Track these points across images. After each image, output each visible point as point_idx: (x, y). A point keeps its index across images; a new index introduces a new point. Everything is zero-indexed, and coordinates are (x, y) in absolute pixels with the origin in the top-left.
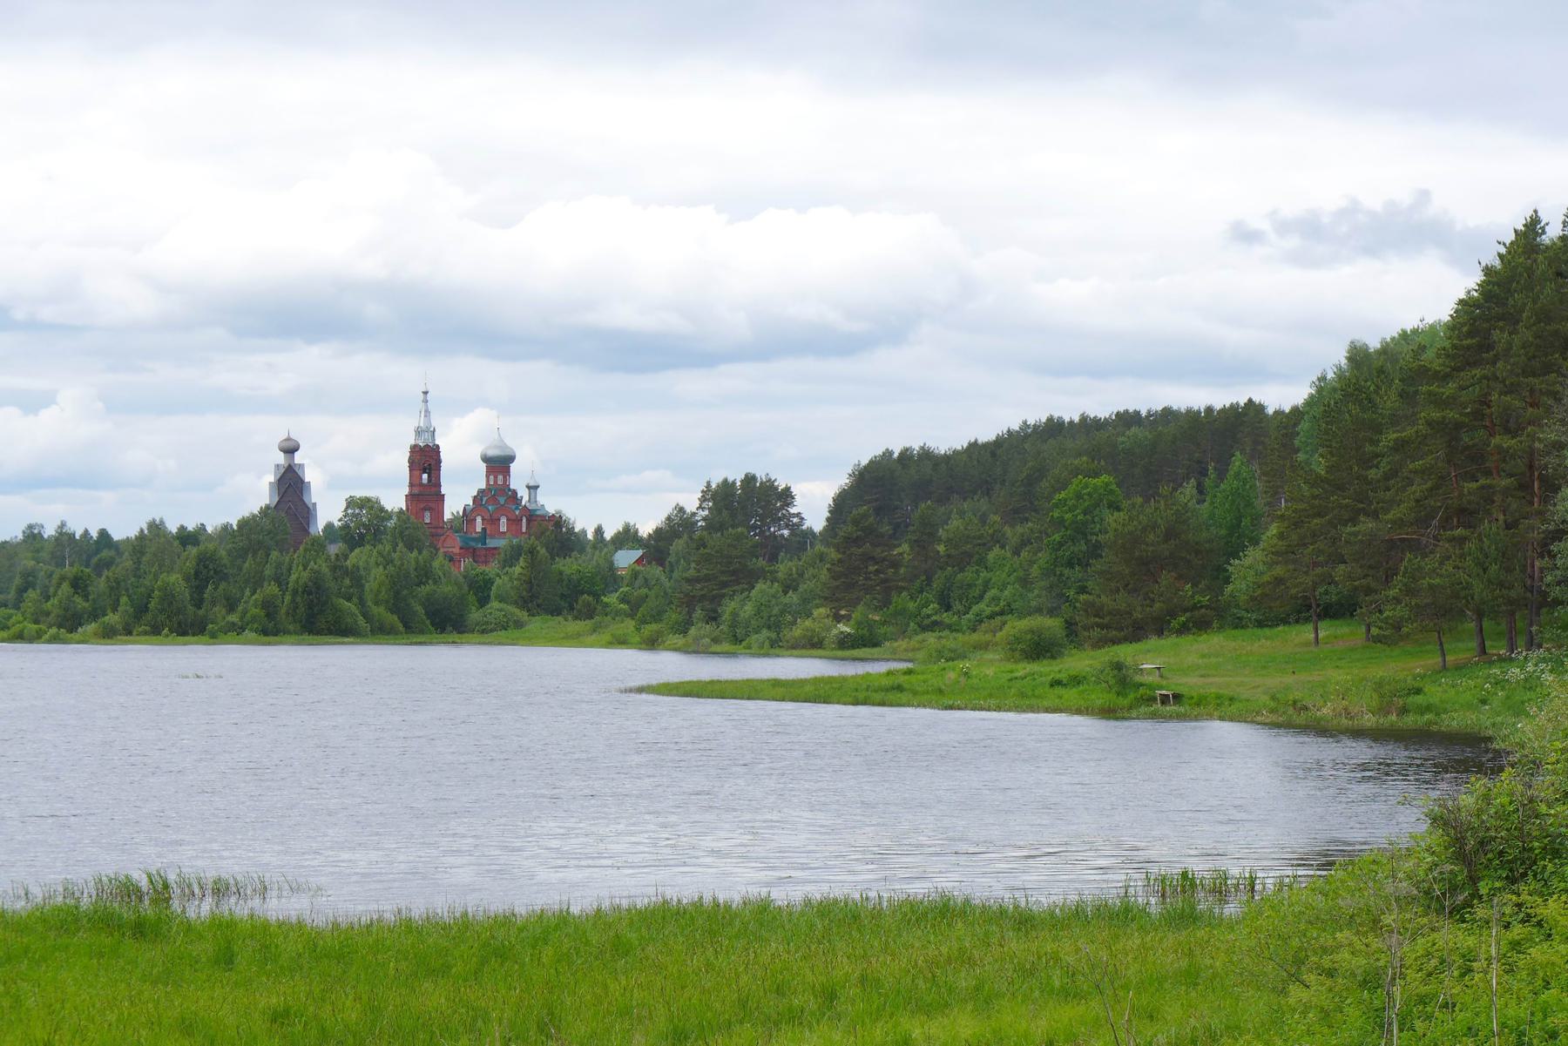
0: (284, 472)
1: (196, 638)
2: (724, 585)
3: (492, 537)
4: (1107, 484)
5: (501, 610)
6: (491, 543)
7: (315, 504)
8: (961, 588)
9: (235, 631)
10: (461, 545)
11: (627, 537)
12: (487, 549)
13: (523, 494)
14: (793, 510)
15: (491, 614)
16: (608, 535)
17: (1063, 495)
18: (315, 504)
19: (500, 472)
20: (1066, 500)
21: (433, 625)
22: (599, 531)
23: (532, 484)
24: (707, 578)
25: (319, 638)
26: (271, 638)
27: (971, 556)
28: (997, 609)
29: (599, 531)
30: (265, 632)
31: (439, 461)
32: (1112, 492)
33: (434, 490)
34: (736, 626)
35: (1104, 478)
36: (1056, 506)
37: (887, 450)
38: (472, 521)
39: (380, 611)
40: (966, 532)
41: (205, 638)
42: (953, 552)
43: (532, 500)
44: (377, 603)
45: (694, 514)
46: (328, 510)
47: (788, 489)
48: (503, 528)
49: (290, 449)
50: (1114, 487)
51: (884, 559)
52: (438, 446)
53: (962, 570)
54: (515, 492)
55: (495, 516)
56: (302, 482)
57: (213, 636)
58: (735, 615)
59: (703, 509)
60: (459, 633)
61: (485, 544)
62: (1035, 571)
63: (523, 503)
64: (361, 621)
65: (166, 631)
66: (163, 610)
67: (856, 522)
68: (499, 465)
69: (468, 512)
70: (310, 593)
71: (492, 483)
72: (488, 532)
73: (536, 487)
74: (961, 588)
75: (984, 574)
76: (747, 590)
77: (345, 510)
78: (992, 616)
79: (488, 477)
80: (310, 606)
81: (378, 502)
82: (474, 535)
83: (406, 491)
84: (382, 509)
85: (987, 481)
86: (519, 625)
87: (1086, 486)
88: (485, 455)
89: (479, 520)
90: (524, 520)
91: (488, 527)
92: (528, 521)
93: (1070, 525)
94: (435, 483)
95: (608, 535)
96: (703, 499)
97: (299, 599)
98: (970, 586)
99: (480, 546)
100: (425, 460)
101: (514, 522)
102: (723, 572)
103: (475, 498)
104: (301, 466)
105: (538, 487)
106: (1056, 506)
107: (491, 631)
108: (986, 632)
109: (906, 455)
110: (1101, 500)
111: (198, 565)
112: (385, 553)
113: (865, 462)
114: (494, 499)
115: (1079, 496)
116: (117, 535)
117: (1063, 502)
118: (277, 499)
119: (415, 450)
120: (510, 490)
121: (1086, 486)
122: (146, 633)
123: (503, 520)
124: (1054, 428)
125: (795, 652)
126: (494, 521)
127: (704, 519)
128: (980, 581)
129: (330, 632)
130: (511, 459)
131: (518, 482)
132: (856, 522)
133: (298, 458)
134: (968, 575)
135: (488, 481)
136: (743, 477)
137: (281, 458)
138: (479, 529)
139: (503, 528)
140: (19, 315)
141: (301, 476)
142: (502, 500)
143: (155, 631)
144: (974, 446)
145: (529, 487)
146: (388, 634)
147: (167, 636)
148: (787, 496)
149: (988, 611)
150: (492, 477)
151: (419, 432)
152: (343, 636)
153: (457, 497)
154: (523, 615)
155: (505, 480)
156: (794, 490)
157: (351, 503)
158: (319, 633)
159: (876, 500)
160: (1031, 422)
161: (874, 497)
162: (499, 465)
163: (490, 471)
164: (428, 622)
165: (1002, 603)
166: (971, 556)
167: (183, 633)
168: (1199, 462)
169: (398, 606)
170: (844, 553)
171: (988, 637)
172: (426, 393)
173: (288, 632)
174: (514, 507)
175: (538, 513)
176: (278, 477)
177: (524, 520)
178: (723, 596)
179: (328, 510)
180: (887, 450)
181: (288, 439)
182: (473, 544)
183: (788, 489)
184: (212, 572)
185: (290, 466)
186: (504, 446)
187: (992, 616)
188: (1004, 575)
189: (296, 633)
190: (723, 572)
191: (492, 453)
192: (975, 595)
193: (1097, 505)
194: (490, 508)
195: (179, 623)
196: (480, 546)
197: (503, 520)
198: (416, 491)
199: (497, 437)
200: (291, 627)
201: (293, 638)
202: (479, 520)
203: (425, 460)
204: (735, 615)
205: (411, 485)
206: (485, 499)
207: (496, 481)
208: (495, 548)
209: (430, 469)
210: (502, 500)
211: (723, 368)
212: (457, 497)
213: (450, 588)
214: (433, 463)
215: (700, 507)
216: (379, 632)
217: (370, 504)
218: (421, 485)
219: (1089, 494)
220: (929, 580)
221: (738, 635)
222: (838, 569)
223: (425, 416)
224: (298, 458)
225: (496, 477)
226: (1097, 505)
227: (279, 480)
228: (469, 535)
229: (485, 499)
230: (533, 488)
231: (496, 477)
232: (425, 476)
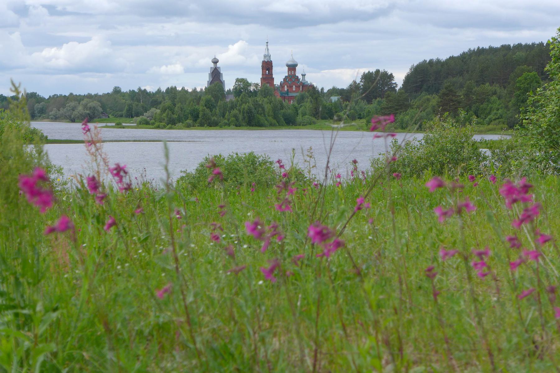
0: (214, 70)
1: (215, 127)
2: (397, 110)
3: (291, 92)
4: (535, 75)
5: (309, 118)
6: (290, 94)
7: (224, 81)
8: (482, 110)
9: (228, 125)
10: (280, 95)
11: (334, 91)
12: (289, 97)
13: (300, 77)
14: (393, 82)
15: (305, 119)
16: (325, 91)
17: (520, 78)
18: (224, 81)
19: (293, 70)
20: (521, 80)
21: (286, 123)
22: (322, 89)
23: (303, 74)
24: (391, 107)
25: (254, 128)
26: (238, 128)
27: (485, 99)
28: (497, 117)
29: (322, 89)
30: (236, 126)
31: (272, 66)
32: (536, 78)
33: (270, 76)
34: (403, 123)
35: (534, 73)
36: (518, 82)
37: (425, 60)
38: (283, 87)
39: (270, 118)
40: (483, 91)
41: (218, 127)
42: (479, 98)
43: (304, 79)
44: (269, 116)
45: (359, 84)
46: (229, 84)
47: (391, 74)
48: (294, 89)
49: (215, 62)
50: (537, 76)
51: (456, 101)
52: (272, 61)
53: (482, 104)
54: (298, 77)
55: (291, 85)
56: (220, 73)
57: (221, 127)
58: (402, 120)
59: (362, 82)
60: (295, 126)
61: (288, 95)
62: (510, 104)
63: (300, 81)
64: (266, 122)
65: (206, 125)
66: (204, 118)
67: (446, 88)
68: (292, 68)
69: (282, 84)
70: (248, 113)
71: (290, 74)
72: (289, 91)
73: (305, 75)
74: (482, 110)
75: (490, 105)
76: (405, 111)
77: (235, 83)
78: (495, 120)
79: (288, 71)
80: (249, 117)
81: (246, 80)
82: (284, 92)
83: (261, 77)
84: (248, 82)
85: (461, 71)
86: (314, 123)
87: (528, 76)
88: (288, 64)
89: (286, 86)
90: (301, 87)
91: (289, 89)
92: (302, 87)
93: (523, 89)
94: (271, 74)
95: (325, 91)
96: (362, 79)
97: (245, 115)
98: (485, 109)
99: (286, 95)
100: (267, 66)
101: (298, 87)
102: (396, 105)
103: (284, 79)
104: (219, 68)
105: (305, 75)
106: (518, 82)
107: (305, 125)
108: (494, 125)
109: (431, 61)
110: (533, 80)
111: (206, 102)
112: (270, 99)
113: (415, 64)
114: (291, 80)
115: (526, 79)
116: (110, 92)
117: (520, 81)
118: (211, 79)
119: (264, 62)
120: (296, 76)
121: (528, 76)
122: (198, 126)
123: (294, 87)
124: (481, 51)
125: (489, 132)
126: (291, 87)
127: (363, 85)
128: (489, 107)
129: (256, 126)
130: (296, 65)
131: (299, 74)
132: (446, 88)
133: (218, 65)
134: (484, 105)
135: (288, 73)
136: (375, 70)
137: (212, 65)
138: (286, 89)
139: (294, 89)
140: (59, 8)
141: (219, 70)
142: (293, 79)
143: (202, 125)
144: (452, 58)
145: (302, 75)
146: (273, 126)
147: (206, 127)
148: (391, 77)
149: (494, 118)
150: (290, 72)
151: (265, 56)
152: (261, 127)
153: (278, 79)
154: (314, 119)
155: (294, 73)
156: (394, 75)
157: (238, 80)
158: (252, 126)
159: (421, 78)
160: (472, 49)
161: (421, 77)
162: (292, 68)
163: (289, 70)
164: (284, 122)
165: (498, 115)
166: (485, 99)
167: (211, 126)
168: (542, 64)
169: (275, 117)
170: (442, 99)
171: (495, 126)
172: (267, 43)
173: (243, 126)
174: (297, 82)
175: (305, 84)
176: (212, 71)
177: (301, 87)
178: (397, 113)
179: (229, 84)
180: (425, 60)
181: (215, 58)
182: (284, 95)
183: (391, 74)
184: (210, 105)
185: (216, 68)
186: (294, 61)
187: (495, 120)
188: (497, 106)
189: (245, 126)
190: (396, 105)
191: (290, 63)
192: (487, 112)
193: (531, 82)
194: (289, 82)
195: (209, 123)
196: (286, 95)
197: (294, 87)
198: (264, 76)
199: (291, 58)
200: (244, 124)
201: (245, 128)
202: (286, 86)
203: (267, 66)
204: (402, 120)
205: (263, 75)
206: (288, 79)
207: (291, 73)
208: (292, 96)
209: (269, 69)
210: (293, 79)
211: (322, 26)
212: (278, 79)
213: (290, 111)
214: (270, 67)
215: (361, 81)
216: (272, 126)
217: (244, 81)
218: (266, 75)
219: (529, 78)
220: (470, 107)
221: (404, 127)
222: (440, 104)
223: (267, 51)
224: (218, 65)
225: (291, 72)
226: (531, 82)
227: (212, 73)
228: (282, 92)
229: (288, 79)
230: (304, 75)
231: (291, 72)
232: (267, 71)
